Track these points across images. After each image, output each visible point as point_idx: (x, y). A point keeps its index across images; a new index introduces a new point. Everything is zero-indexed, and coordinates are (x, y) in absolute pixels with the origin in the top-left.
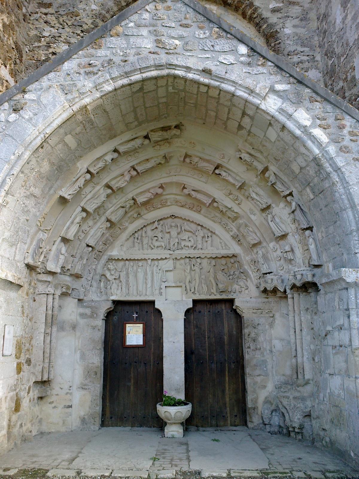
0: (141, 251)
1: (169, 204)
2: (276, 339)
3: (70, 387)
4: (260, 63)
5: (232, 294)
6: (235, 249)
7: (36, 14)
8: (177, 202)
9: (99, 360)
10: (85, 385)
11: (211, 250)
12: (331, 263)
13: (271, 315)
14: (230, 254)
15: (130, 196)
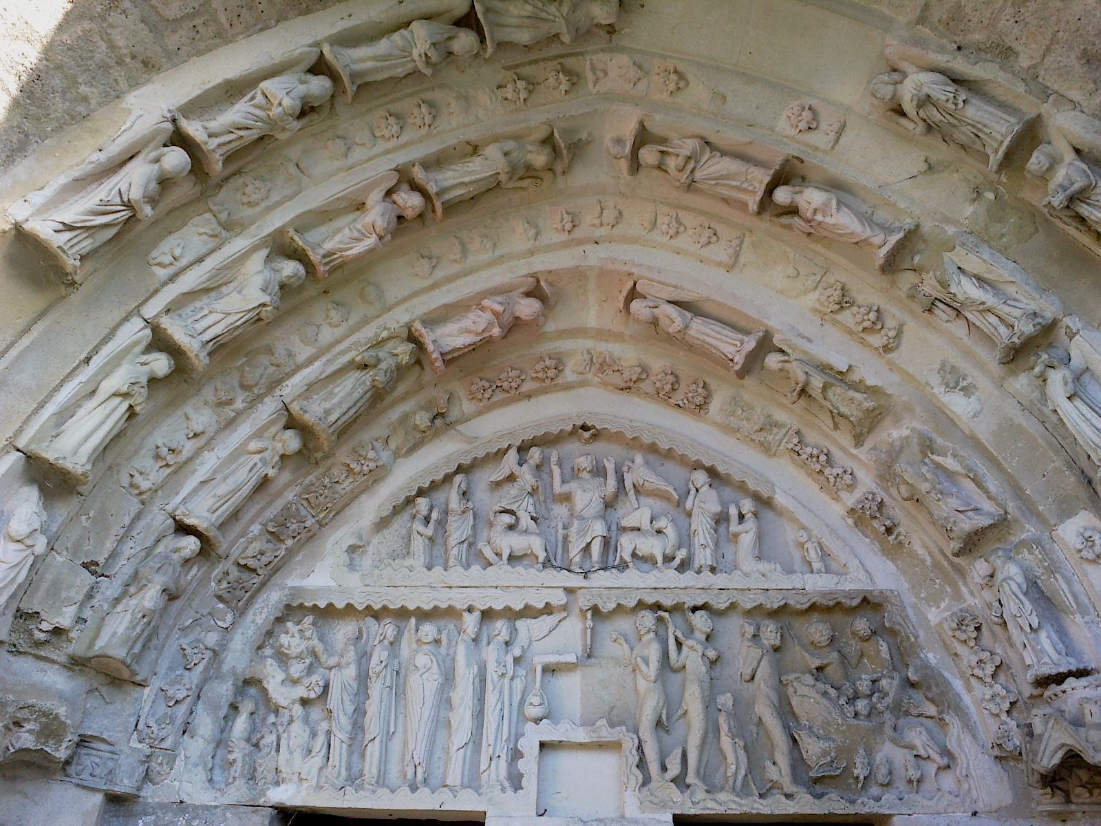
1: (569, 375)
11: (754, 577)
14: (850, 594)
15: (399, 318)
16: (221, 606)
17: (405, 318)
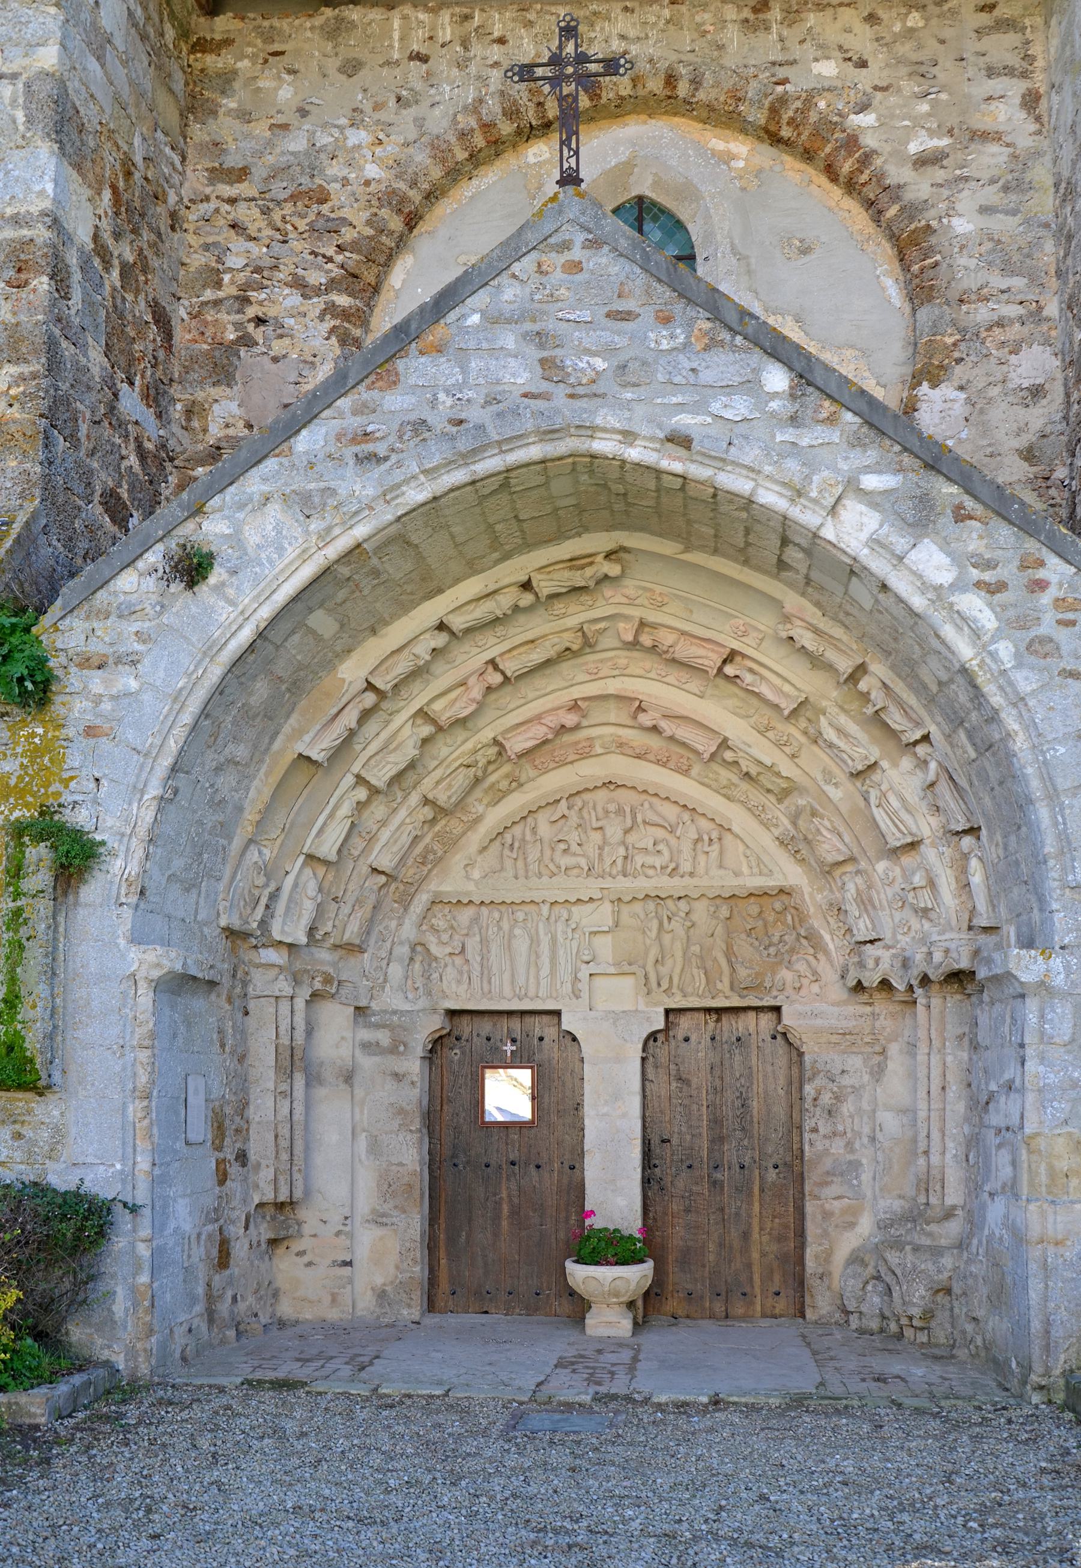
0: (522, 880)
2: (888, 1108)
3: (346, 1218)
4: (824, 415)
6: (790, 873)
7: (205, 205)
8: (621, 745)
9: (417, 1157)
10: (383, 1215)
13: (878, 1049)
14: (772, 888)
15: (487, 735)
17: (491, 735)
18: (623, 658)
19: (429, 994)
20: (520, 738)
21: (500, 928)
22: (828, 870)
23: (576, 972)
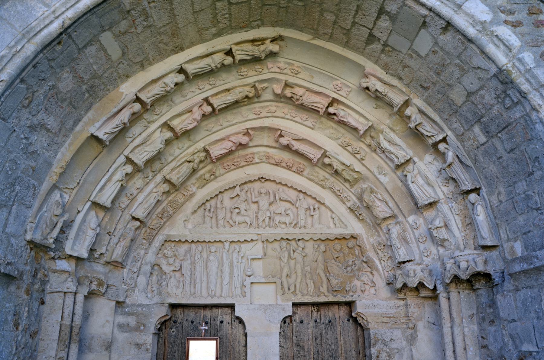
0: (215, 229)
5: (351, 294)
6: (355, 227)
12: (519, 242)
13: (411, 325)
14: (347, 235)
15: (200, 145)
16: (145, 241)
17: (203, 145)
18: (273, 106)
19: (160, 294)
20: (218, 148)
21: (202, 256)
22: (377, 223)
23: (243, 281)
